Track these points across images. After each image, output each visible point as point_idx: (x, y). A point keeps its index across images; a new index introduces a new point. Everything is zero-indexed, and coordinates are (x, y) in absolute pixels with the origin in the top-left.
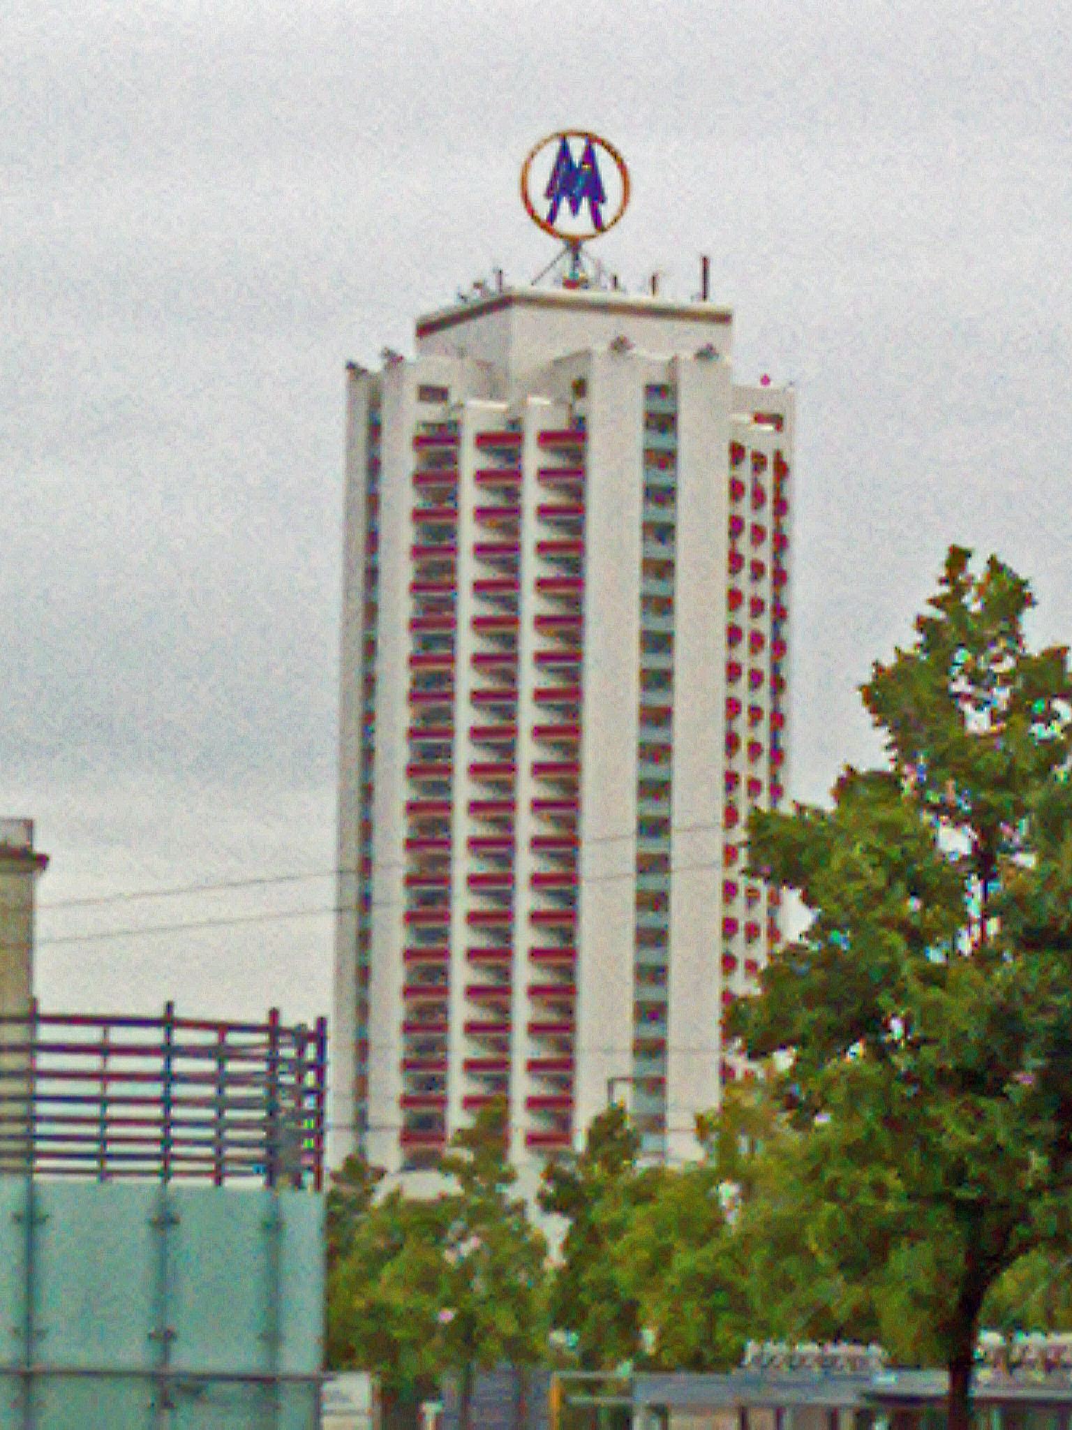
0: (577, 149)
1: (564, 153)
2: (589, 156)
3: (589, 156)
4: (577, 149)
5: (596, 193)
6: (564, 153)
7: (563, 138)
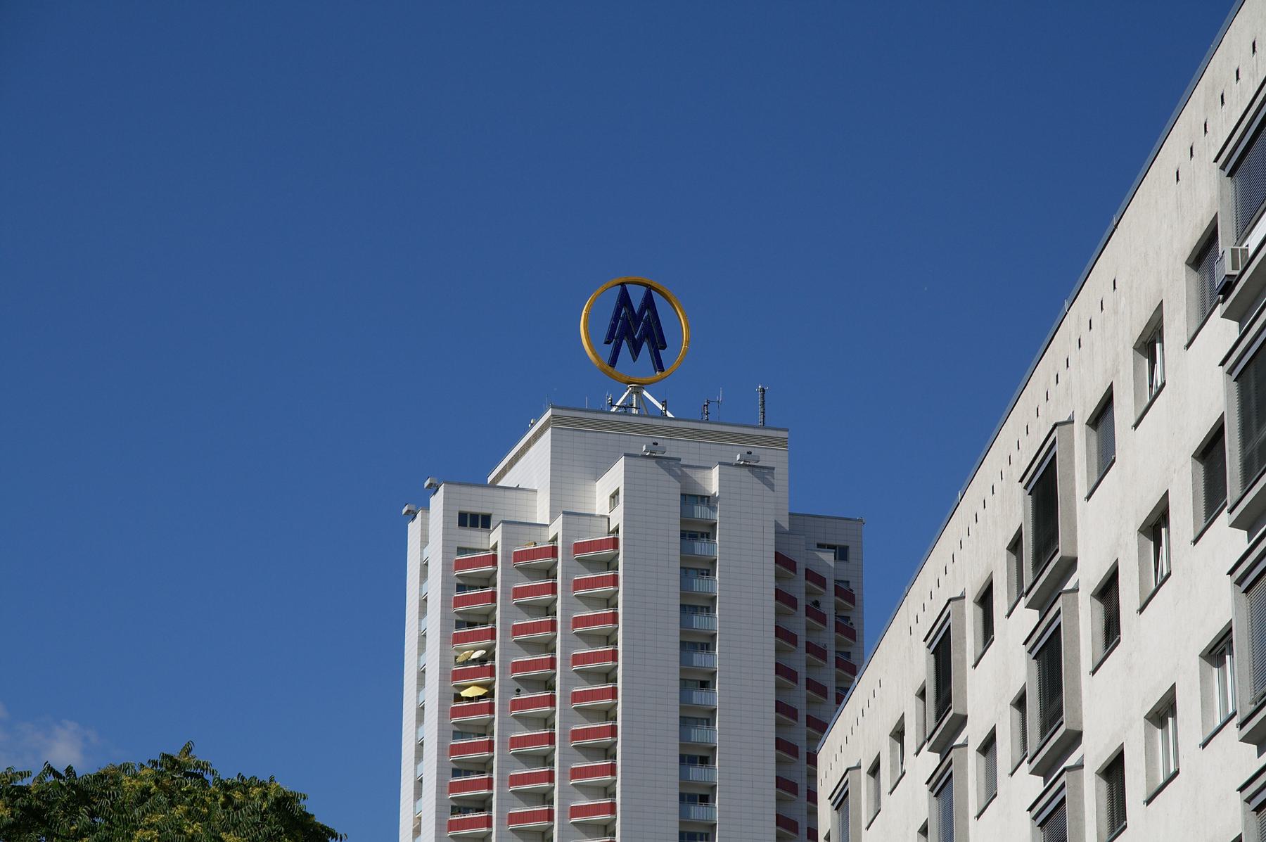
1: (624, 299)
2: (649, 302)
3: (649, 302)
5: (658, 343)
6: (624, 299)
7: (623, 284)
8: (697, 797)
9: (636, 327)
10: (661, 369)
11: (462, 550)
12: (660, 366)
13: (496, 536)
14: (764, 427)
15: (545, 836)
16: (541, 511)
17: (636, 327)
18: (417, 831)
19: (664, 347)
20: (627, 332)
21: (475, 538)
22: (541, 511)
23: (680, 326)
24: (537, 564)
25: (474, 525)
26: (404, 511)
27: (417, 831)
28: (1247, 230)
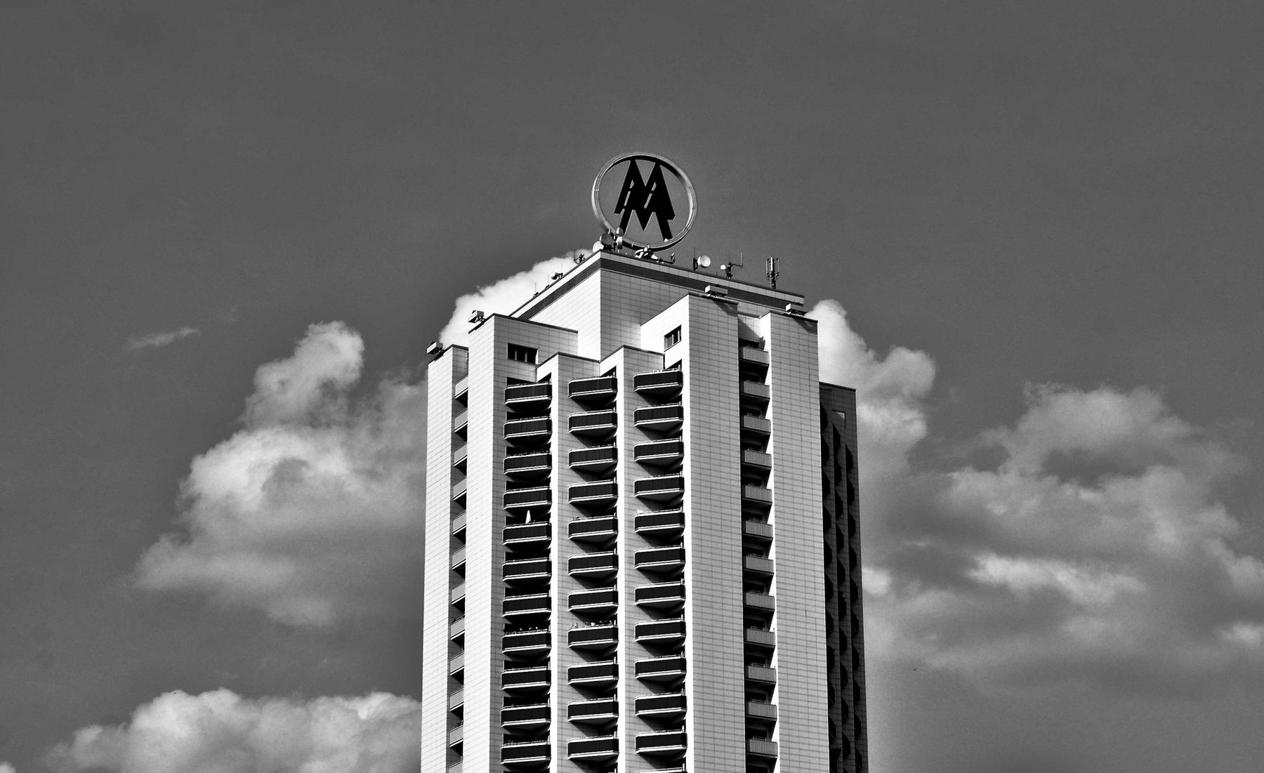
0: (646, 171)
1: (633, 173)
2: (657, 176)
3: (657, 176)
4: (646, 171)
5: (665, 211)
6: (633, 173)
7: (633, 159)
8: (759, 728)
9: (646, 197)
10: (669, 237)
11: (511, 381)
12: (667, 233)
13: (551, 368)
14: (774, 289)
15: (611, 763)
16: (588, 345)
17: (646, 197)
18: (456, 752)
19: (672, 216)
20: (636, 203)
21: (525, 372)
22: (588, 345)
23: (687, 200)
24: (595, 397)
25: (521, 359)
26: (430, 349)
27: (456, 752)
28: (831, 442)
